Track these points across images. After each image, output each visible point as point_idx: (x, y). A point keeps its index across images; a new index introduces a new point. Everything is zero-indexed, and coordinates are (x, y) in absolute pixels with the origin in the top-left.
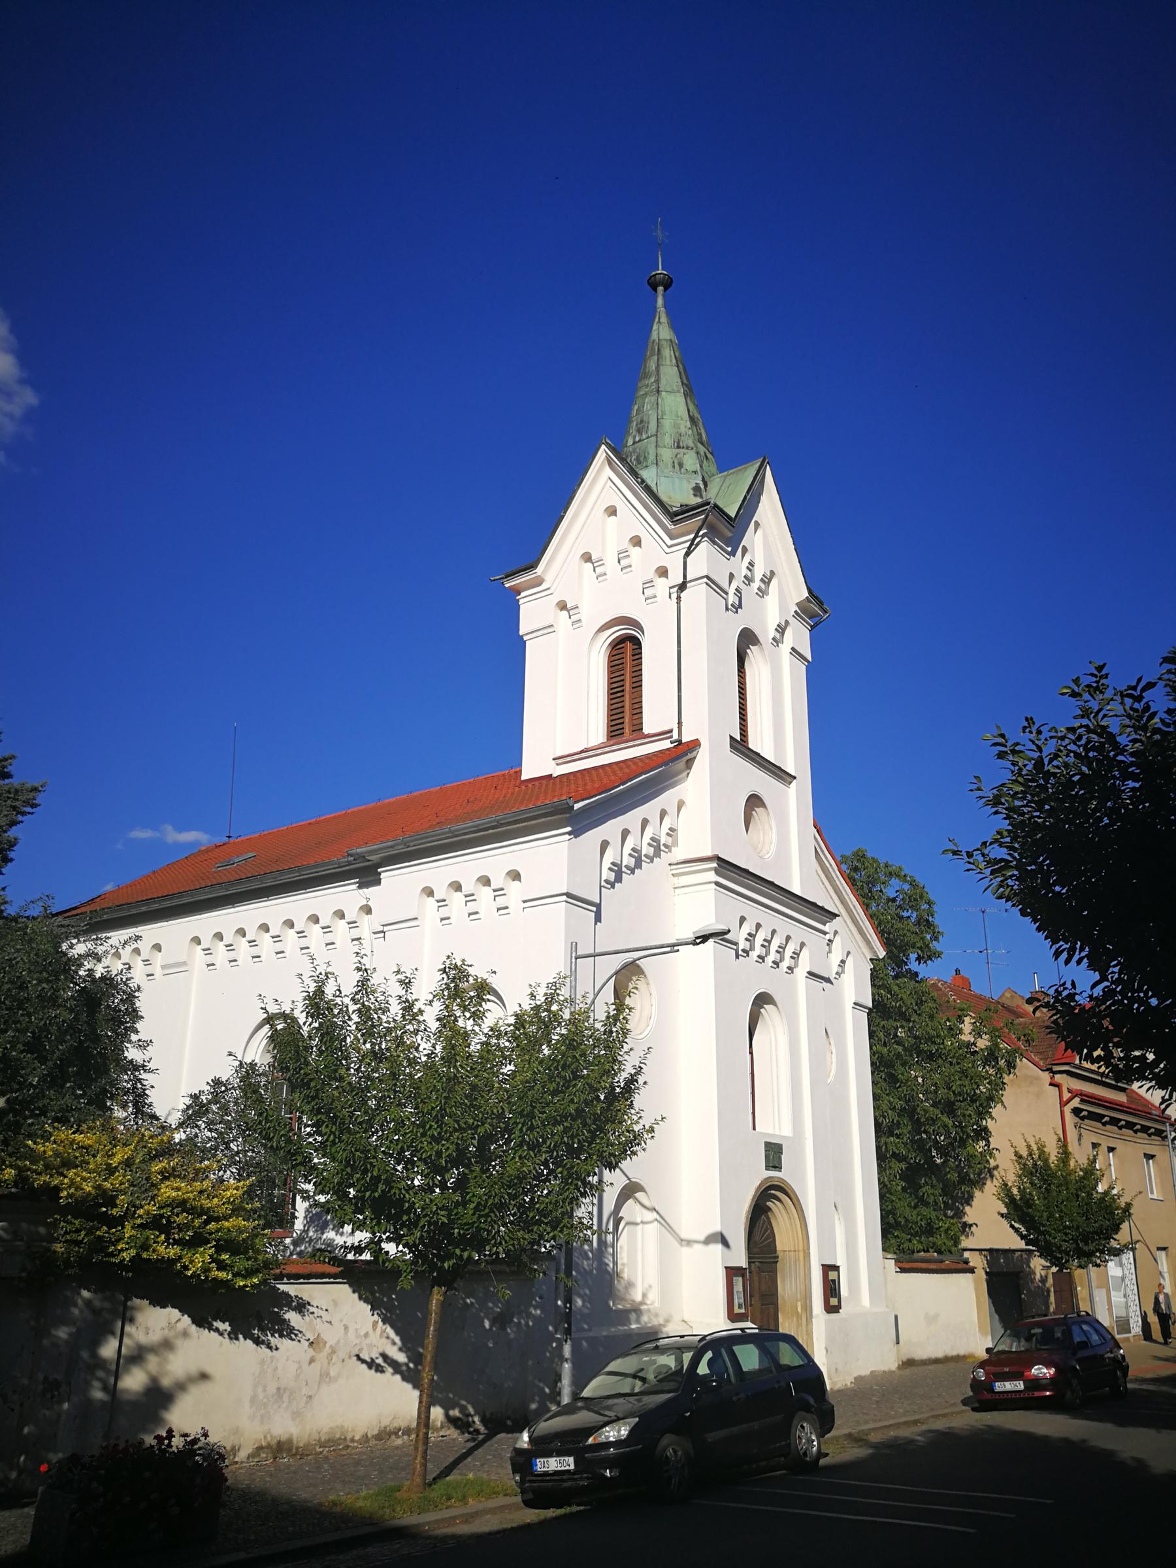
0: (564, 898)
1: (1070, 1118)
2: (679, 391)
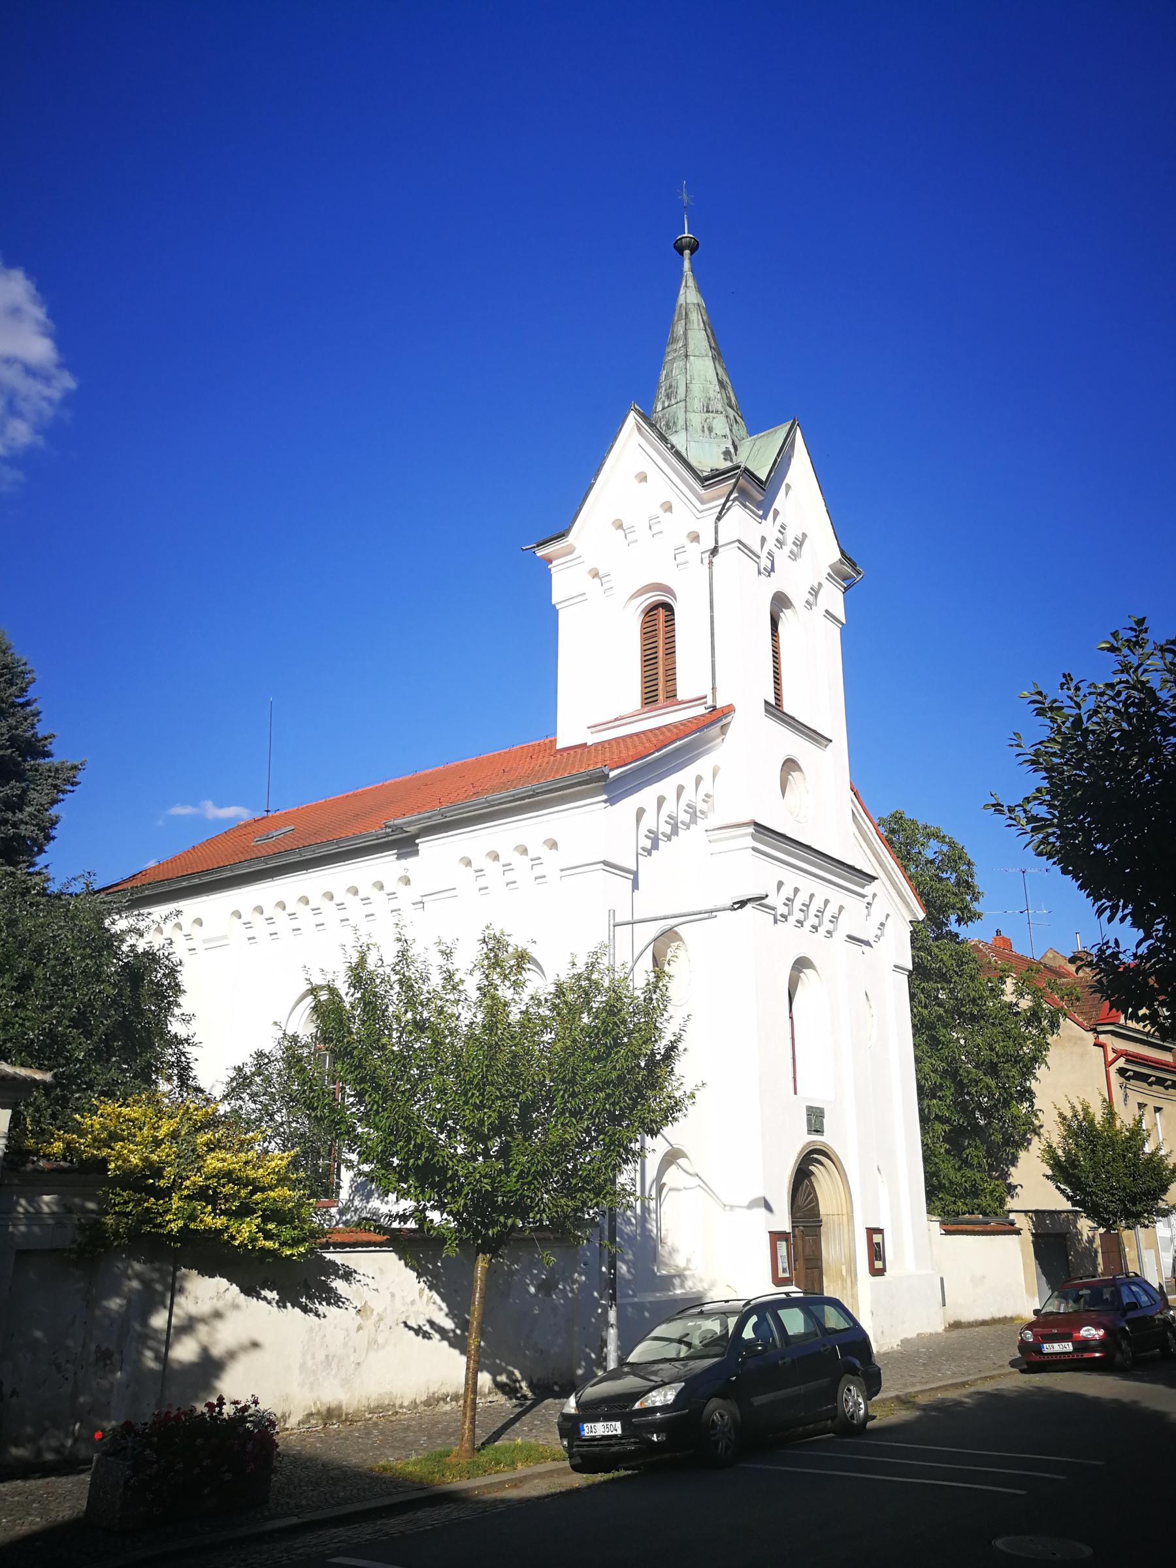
0: (602, 866)
1: (1115, 1079)
2: (707, 355)
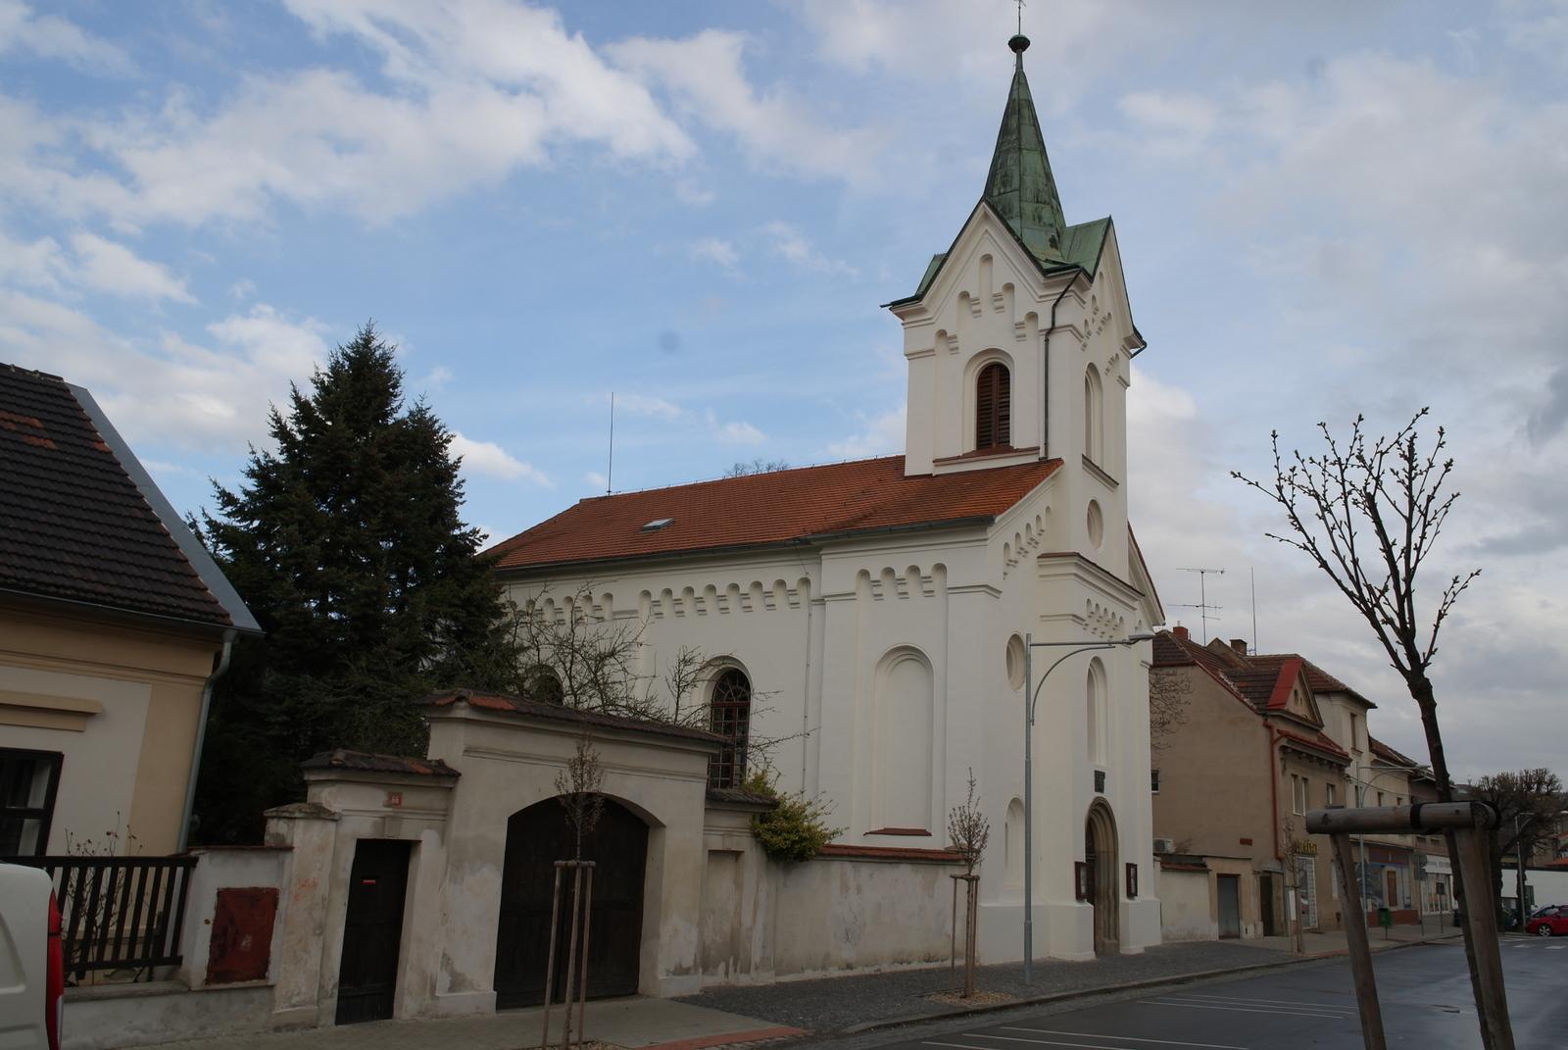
0: (1071, 617)
1: (1278, 754)
2: (1036, 150)
